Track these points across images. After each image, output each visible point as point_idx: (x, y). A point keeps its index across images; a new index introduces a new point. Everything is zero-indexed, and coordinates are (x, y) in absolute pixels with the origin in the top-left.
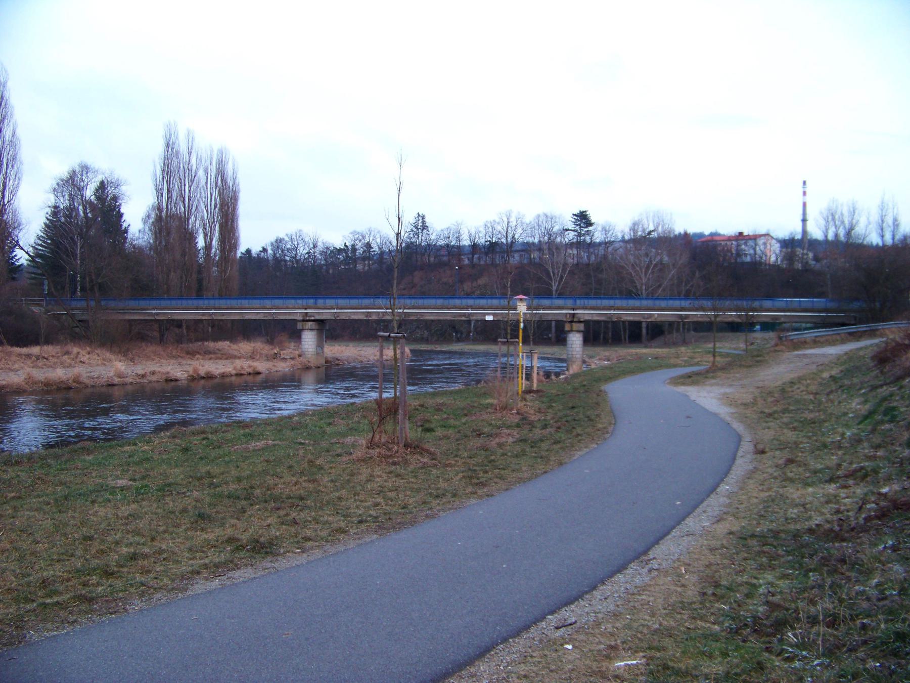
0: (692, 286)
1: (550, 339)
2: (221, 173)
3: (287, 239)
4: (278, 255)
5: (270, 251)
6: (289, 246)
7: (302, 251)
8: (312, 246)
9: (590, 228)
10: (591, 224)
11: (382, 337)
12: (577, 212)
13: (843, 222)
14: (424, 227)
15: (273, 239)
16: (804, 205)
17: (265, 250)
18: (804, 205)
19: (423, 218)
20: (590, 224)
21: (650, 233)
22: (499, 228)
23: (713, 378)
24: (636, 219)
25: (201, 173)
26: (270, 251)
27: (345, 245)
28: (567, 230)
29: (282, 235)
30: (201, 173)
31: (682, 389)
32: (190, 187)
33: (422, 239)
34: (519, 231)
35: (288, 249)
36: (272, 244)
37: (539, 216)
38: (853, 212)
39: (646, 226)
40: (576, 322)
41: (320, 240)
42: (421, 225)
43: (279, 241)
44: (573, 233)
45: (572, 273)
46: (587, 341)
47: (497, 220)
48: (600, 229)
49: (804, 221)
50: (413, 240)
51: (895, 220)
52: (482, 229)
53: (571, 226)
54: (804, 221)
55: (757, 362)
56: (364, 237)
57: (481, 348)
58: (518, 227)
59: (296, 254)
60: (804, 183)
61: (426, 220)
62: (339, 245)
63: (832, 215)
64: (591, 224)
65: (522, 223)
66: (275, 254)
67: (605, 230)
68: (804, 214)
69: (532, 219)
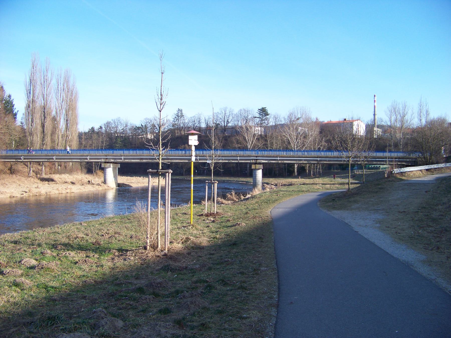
0: (321, 146)
1: (246, 173)
2: (67, 81)
3: (112, 122)
4: (108, 130)
5: (104, 128)
6: (113, 126)
7: (120, 128)
8: (125, 126)
9: (268, 117)
10: (268, 115)
11: (150, 172)
12: (260, 108)
13: (400, 113)
14: (182, 116)
15: (105, 122)
16: (375, 106)
17: (101, 128)
18: (375, 106)
19: (181, 111)
20: (267, 114)
21: (298, 119)
22: (220, 116)
23: (355, 202)
24: (291, 111)
25: (54, 82)
26: (104, 128)
27: (142, 126)
28: (255, 117)
29: (110, 120)
30: (54, 82)
31: (337, 214)
32: (47, 89)
33: (181, 123)
34: (231, 118)
35: (113, 127)
36: (105, 124)
37: (241, 110)
38: (405, 107)
39: (296, 115)
40: (258, 164)
41: (129, 122)
42: (180, 115)
43: (108, 124)
44: (259, 119)
45: (258, 139)
46: (265, 175)
47: (220, 112)
48: (272, 117)
49: (374, 115)
50: (176, 123)
51: (427, 111)
52: (212, 117)
53: (257, 115)
54: (374, 115)
55: (380, 188)
56: (151, 121)
57: (227, 179)
58: (230, 116)
59: (117, 130)
60: (375, 96)
61: (183, 112)
62: (138, 125)
63: (394, 108)
64: (268, 115)
65: (232, 114)
66: (106, 130)
67: (275, 118)
68: (375, 111)
69: (237, 112)
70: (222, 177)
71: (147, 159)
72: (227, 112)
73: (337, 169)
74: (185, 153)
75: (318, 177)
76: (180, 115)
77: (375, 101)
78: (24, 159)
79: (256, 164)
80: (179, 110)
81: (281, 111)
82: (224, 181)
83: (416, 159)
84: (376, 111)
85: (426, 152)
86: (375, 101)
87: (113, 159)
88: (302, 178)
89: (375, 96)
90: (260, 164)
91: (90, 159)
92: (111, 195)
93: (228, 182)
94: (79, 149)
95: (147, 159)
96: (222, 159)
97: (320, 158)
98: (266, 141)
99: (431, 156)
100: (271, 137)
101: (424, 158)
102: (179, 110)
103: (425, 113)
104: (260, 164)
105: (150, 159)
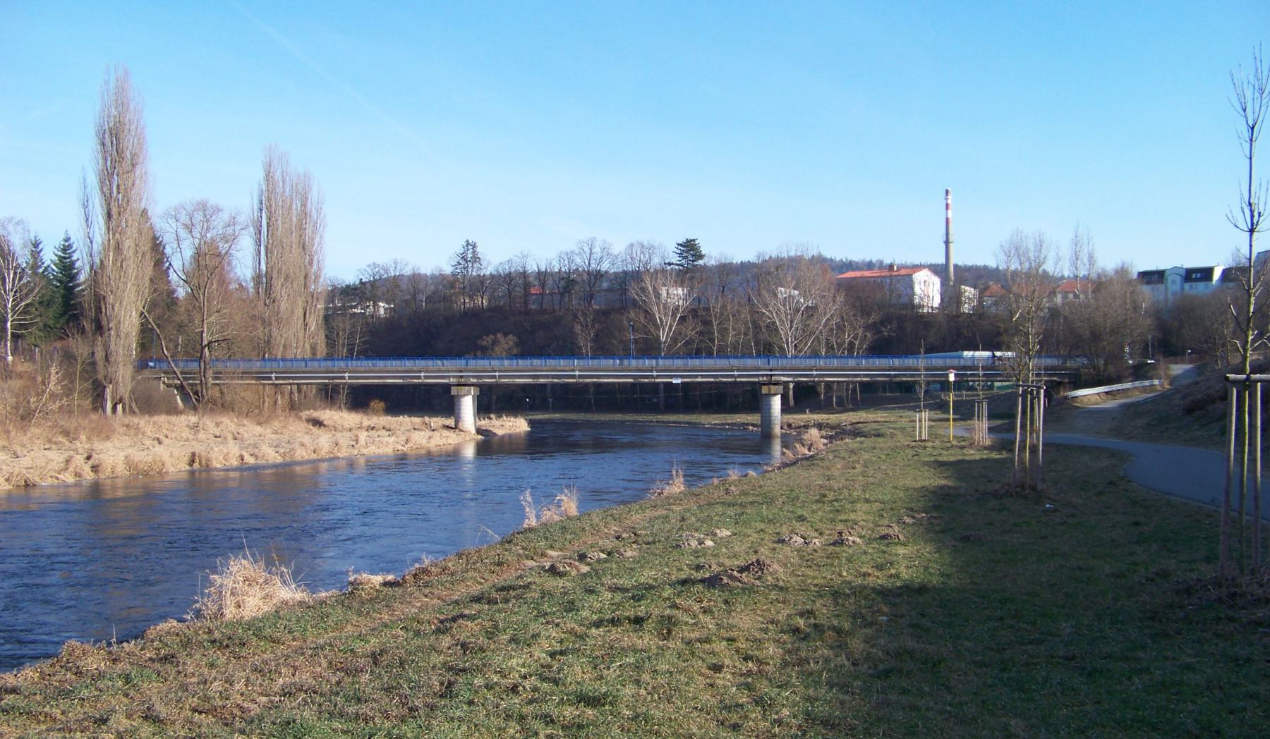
10: (701, 257)
14: (476, 259)
16: (947, 220)
18: (947, 220)
19: (474, 246)
37: (632, 245)
38: (1040, 245)
42: (470, 254)
51: (1091, 257)
60: (947, 192)
69: (622, 250)
70: (592, 412)
71: (547, 377)
72: (597, 250)
73: (891, 392)
74: (621, 364)
75: (852, 410)
76: (470, 254)
77: (947, 205)
78: (277, 378)
79: (770, 383)
80: (468, 244)
81: (731, 243)
82: (623, 422)
83: (1078, 369)
84: (951, 232)
85: (1098, 356)
86: (947, 205)
87: (474, 377)
88: (812, 411)
89: (947, 192)
90: (776, 384)
91: (426, 377)
92: (469, 452)
93: (605, 425)
94: (330, 357)
95: (547, 377)
96: (703, 376)
97: (894, 370)
98: (707, 323)
99: (1106, 363)
100: (722, 314)
101: (1094, 368)
102: (468, 244)
103: (1086, 260)
104: (776, 384)
105: (554, 376)
